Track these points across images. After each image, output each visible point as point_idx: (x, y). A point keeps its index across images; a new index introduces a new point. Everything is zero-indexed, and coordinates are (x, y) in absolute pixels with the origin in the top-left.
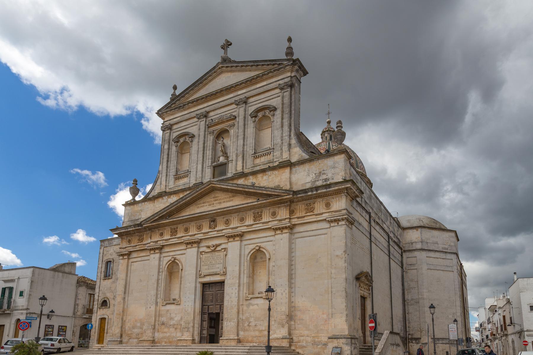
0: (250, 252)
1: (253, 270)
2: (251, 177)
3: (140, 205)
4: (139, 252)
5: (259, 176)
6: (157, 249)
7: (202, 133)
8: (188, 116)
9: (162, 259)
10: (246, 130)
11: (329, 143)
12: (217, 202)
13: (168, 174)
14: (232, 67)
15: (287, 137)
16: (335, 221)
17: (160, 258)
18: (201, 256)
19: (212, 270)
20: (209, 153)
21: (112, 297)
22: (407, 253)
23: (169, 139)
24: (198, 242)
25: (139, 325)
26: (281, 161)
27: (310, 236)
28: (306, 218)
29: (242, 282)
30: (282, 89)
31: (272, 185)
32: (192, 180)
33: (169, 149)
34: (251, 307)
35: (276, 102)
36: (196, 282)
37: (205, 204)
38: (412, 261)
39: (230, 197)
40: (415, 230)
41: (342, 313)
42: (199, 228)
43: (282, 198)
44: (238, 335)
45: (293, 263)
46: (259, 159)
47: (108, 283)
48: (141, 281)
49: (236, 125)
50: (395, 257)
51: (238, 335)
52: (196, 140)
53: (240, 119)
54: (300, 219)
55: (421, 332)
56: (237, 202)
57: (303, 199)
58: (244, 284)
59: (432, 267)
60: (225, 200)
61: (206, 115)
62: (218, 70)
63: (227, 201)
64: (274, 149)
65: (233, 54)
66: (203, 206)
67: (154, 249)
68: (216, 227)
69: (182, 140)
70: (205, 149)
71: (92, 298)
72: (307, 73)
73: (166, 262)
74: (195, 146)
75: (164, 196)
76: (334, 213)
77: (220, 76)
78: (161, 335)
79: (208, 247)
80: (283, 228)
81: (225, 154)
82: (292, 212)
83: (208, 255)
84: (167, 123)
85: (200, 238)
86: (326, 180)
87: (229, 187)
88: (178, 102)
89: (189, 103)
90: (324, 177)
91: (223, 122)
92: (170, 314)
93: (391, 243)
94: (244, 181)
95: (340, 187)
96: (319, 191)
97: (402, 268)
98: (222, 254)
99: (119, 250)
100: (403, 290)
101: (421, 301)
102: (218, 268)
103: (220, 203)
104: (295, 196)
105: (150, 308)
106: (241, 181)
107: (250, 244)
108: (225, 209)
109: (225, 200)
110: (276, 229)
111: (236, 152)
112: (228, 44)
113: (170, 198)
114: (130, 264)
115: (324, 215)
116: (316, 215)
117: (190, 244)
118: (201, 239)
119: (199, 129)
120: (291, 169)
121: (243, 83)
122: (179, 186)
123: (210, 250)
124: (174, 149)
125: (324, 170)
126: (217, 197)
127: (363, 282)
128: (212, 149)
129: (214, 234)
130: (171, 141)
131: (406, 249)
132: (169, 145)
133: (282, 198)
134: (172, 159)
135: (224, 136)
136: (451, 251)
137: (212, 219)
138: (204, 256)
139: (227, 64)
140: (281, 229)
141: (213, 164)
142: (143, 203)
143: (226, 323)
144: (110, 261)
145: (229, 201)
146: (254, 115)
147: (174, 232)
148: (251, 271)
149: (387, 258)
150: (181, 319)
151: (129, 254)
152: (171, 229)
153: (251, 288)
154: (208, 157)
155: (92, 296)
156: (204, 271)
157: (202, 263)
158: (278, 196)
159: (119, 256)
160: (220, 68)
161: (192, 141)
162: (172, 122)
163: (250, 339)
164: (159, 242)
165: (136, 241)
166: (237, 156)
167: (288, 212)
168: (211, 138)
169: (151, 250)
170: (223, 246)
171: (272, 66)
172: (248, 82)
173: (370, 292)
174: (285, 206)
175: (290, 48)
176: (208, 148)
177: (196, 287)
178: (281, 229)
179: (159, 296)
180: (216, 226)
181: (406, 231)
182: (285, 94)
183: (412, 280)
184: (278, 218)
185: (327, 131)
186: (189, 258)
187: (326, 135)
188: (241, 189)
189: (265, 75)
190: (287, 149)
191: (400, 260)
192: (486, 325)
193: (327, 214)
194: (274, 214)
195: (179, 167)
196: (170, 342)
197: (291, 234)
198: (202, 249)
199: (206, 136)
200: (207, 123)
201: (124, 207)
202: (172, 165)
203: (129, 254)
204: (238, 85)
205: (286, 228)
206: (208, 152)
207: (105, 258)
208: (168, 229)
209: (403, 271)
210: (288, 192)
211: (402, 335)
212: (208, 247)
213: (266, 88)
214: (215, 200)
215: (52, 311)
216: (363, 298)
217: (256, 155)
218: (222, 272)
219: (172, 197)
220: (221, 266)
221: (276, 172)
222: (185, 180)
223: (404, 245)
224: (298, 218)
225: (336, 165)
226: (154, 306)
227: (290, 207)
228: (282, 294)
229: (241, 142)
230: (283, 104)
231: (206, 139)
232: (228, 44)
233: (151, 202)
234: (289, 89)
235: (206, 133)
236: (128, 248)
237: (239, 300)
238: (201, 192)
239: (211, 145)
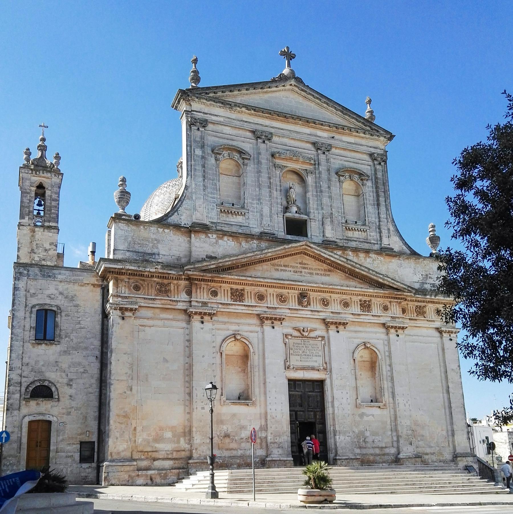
12: (306, 271)
21: (65, 381)
28: (361, 317)
34: (365, 418)
37: (287, 269)
41: (463, 430)
46: (351, 232)
48: (166, 361)
60: (319, 272)
63: (321, 275)
66: (285, 271)
92: (240, 420)
102: (317, 362)
109: (319, 272)
113: (222, 238)
126: (305, 264)
145: (326, 275)
156: (294, 361)
175: (196, 72)
180: (309, 304)
211: (268, 459)
219: (226, 238)
228: (405, 405)
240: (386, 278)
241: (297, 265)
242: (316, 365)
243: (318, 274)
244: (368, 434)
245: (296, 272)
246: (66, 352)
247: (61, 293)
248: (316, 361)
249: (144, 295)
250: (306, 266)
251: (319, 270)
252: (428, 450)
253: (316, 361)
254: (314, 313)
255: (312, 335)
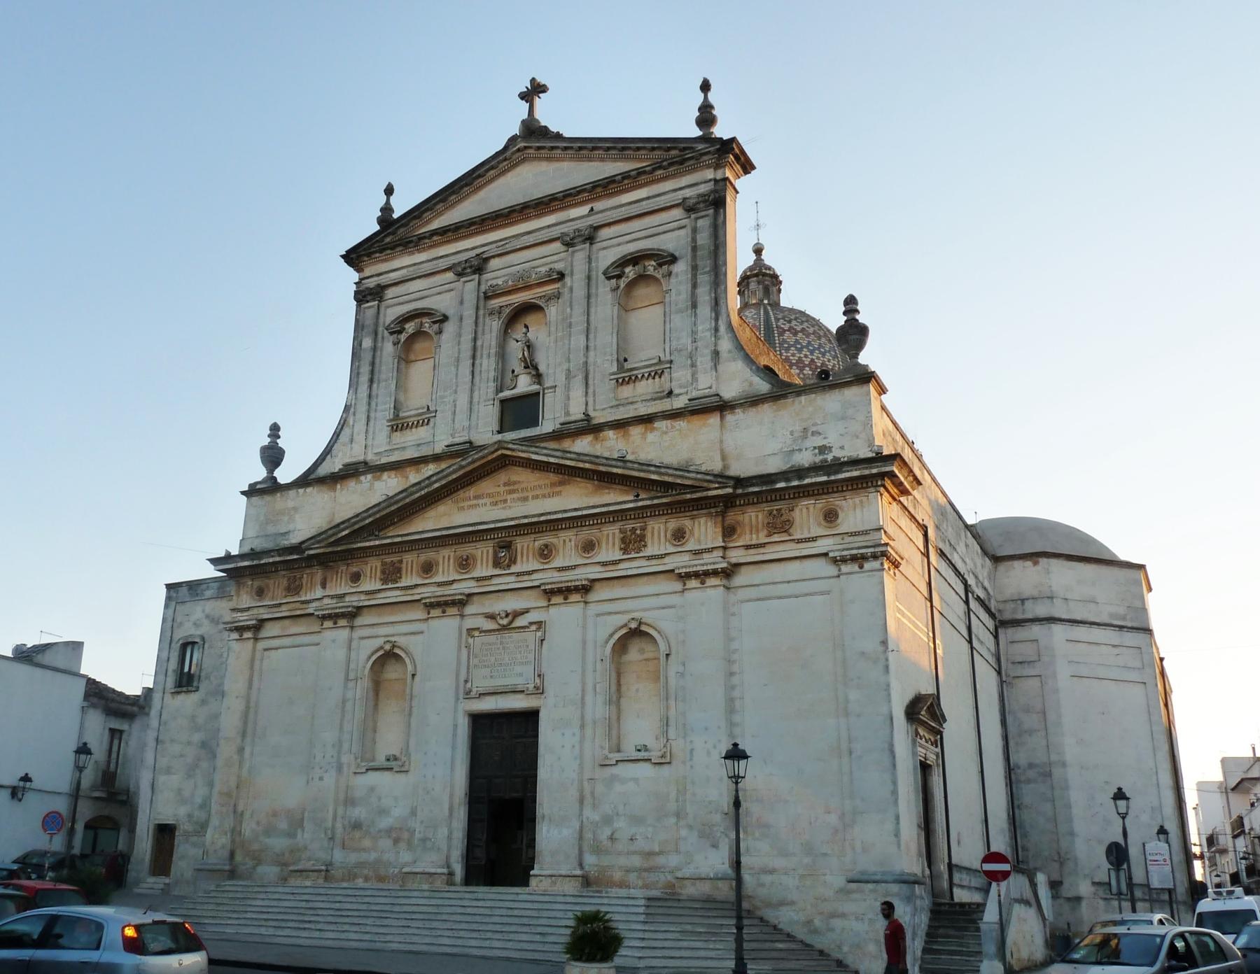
0: (611, 635)
1: (619, 685)
2: (610, 434)
3: (292, 493)
4: (287, 622)
5: (636, 431)
6: (343, 615)
7: (469, 312)
8: (428, 268)
9: (354, 644)
10: (592, 310)
11: (766, 312)
12: (515, 496)
13: (372, 415)
14: (552, 148)
15: (708, 334)
16: (854, 559)
17: (350, 641)
18: (471, 640)
19: (503, 682)
20: (488, 365)
22: (1010, 631)
23: (376, 324)
24: (461, 603)
25: (283, 825)
26: (695, 394)
27: (780, 598)
29: (588, 717)
30: (690, 209)
31: (671, 458)
32: (440, 437)
33: (374, 349)
34: (618, 788)
35: (672, 242)
36: (456, 711)
37: (481, 501)
38: (1026, 651)
39: (553, 485)
40: (1029, 563)
42: (465, 564)
43: (705, 494)
44: (581, 866)
45: (735, 668)
47: (188, 701)
49: (566, 295)
50: (982, 643)
51: (581, 866)
52: (449, 328)
53: (576, 282)
54: (752, 551)
55: (1062, 864)
56: (576, 498)
57: (759, 498)
58: (594, 722)
59: (1084, 671)
61: (478, 266)
62: (513, 154)
63: (544, 496)
64: (671, 362)
65: (549, 114)
67: (334, 617)
68: (515, 563)
69: (410, 327)
70: (478, 354)
71: (116, 742)
72: (753, 168)
73: (369, 652)
74: (451, 343)
75: (364, 473)
76: (848, 539)
77: (519, 170)
78: (353, 858)
79: (491, 617)
80: (707, 574)
81: (531, 366)
82: (729, 532)
83: (492, 638)
84: (371, 283)
85: (467, 591)
86: (823, 449)
87: (552, 460)
88: (402, 230)
89: (434, 233)
90: (819, 442)
91: (528, 287)
92: (380, 799)
93: (974, 604)
94: (591, 443)
95: (867, 472)
96: (807, 481)
97: (999, 673)
98: (531, 637)
99: (228, 617)
100: (1006, 738)
101: (1057, 772)
102: (522, 676)
103: (525, 499)
104: (740, 491)
105: (321, 779)
106: (582, 445)
107: (610, 613)
108: (542, 518)
110: (685, 577)
111: (565, 366)
112: (535, 90)
113: (379, 479)
114: (258, 655)
115: (820, 542)
116: (799, 541)
117: (442, 605)
118: (470, 595)
119: (462, 303)
120: (722, 418)
121: (584, 191)
122: (404, 448)
123: (495, 626)
124: (388, 348)
125: (815, 424)
126: (515, 483)
127: (923, 723)
128: (497, 354)
129: (509, 582)
130: (381, 329)
131: (1007, 616)
132: (375, 340)
133: (705, 494)
134: (383, 376)
135: (531, 319)
136: (1135, 625)
137: (504, 540)
138: (479, 640)
139: (535, 139)
140: (702, 576)
141: (502, 395)
142: (301, 491)
143: (545, 829)
144: (194, 643)
146: (615, 271)
147: (391, 574)
148: (614, 688)
149: (966, 646)
150: (414, 813)
151: (260, 625)
152: (384, 564)
153: (614, 732)
154: (484, 375)
155: (117, 735)
156: (481, 682)
157: (474, 661)
158: (693, 488)
159: (231, 630)
160: (519, 150)
161: (440, 332)
162: (383, 280)
163: (618, 875)
164: (347, 599)
165: (280, 592)
166: (569, 375)
167: (719, 530)
168: (495, 325)
169: (324, 618)
170: (533, 616)
171: (667, 156)
172: (599, 190)
173: (939, 750)
174: (710, 515)
176: (485, 352)
177: (455, 726)
178: (702, 576)
179: (346, 746)
180: (513, 561)
181: (1002, 567)
182: (700, 223)
183: (1027, 710)
184: (691, 545)
185: (756, 275)
186: (434, 644)
187: (753, 285)
188: (587, 466)
189: (645, 172)
190: (710, 364)
191: (993, 648)
192: (1225, 840)
193: (829, 541)
194: (679, 535)
195: (402, 398)
196: (381, 879)
197: (728, 588)
198: (470, 623)
199: (481, 319)
200: (483, 288)
201: (245, 498)
202: (382, 392)
203: (260, 625)
204: (570, 195)
205: (715, 573)
206: (485, 362)
207: (180, 634)
208: (375, 564)
209: (1002, 683)
210: (722, 478)
212: (491, 617)
213: (646, 206)
214: (510, 492)
215: (26, 778)
216: (925, 768)
217: (626, 377)
218: (531, 686)
220: (529, 671)
221: (681, 424)
222: (422, 433)
223: (1001, 607)
224: (748, 547)
225: (850, 412)
226: (333, 773)
227: (723, 517)
228: (709, 753)
229: (579, 341)
230: (694, 249)
231: (480, 329)
232: (535, 90)
233: (324, 488)
234: (711, 212)
235: (481, 312)
236: (255, 611)
237: (581, 766)
238: (471, 468)
239: (494, 343)
240: (663, 470)
241: (498, 489)
242: (518, 681)
243: (536, 497)
244: (620, 824)
245: (496, 504)
246: (204, 702)
247: (207, 617)
248: (521, 675)
249: (273, 599)
250: (516, 487)
251: (540, 487)
252: (779, 863)
253: (521, 675)
254: (520, 578)
255: (520, 622)
